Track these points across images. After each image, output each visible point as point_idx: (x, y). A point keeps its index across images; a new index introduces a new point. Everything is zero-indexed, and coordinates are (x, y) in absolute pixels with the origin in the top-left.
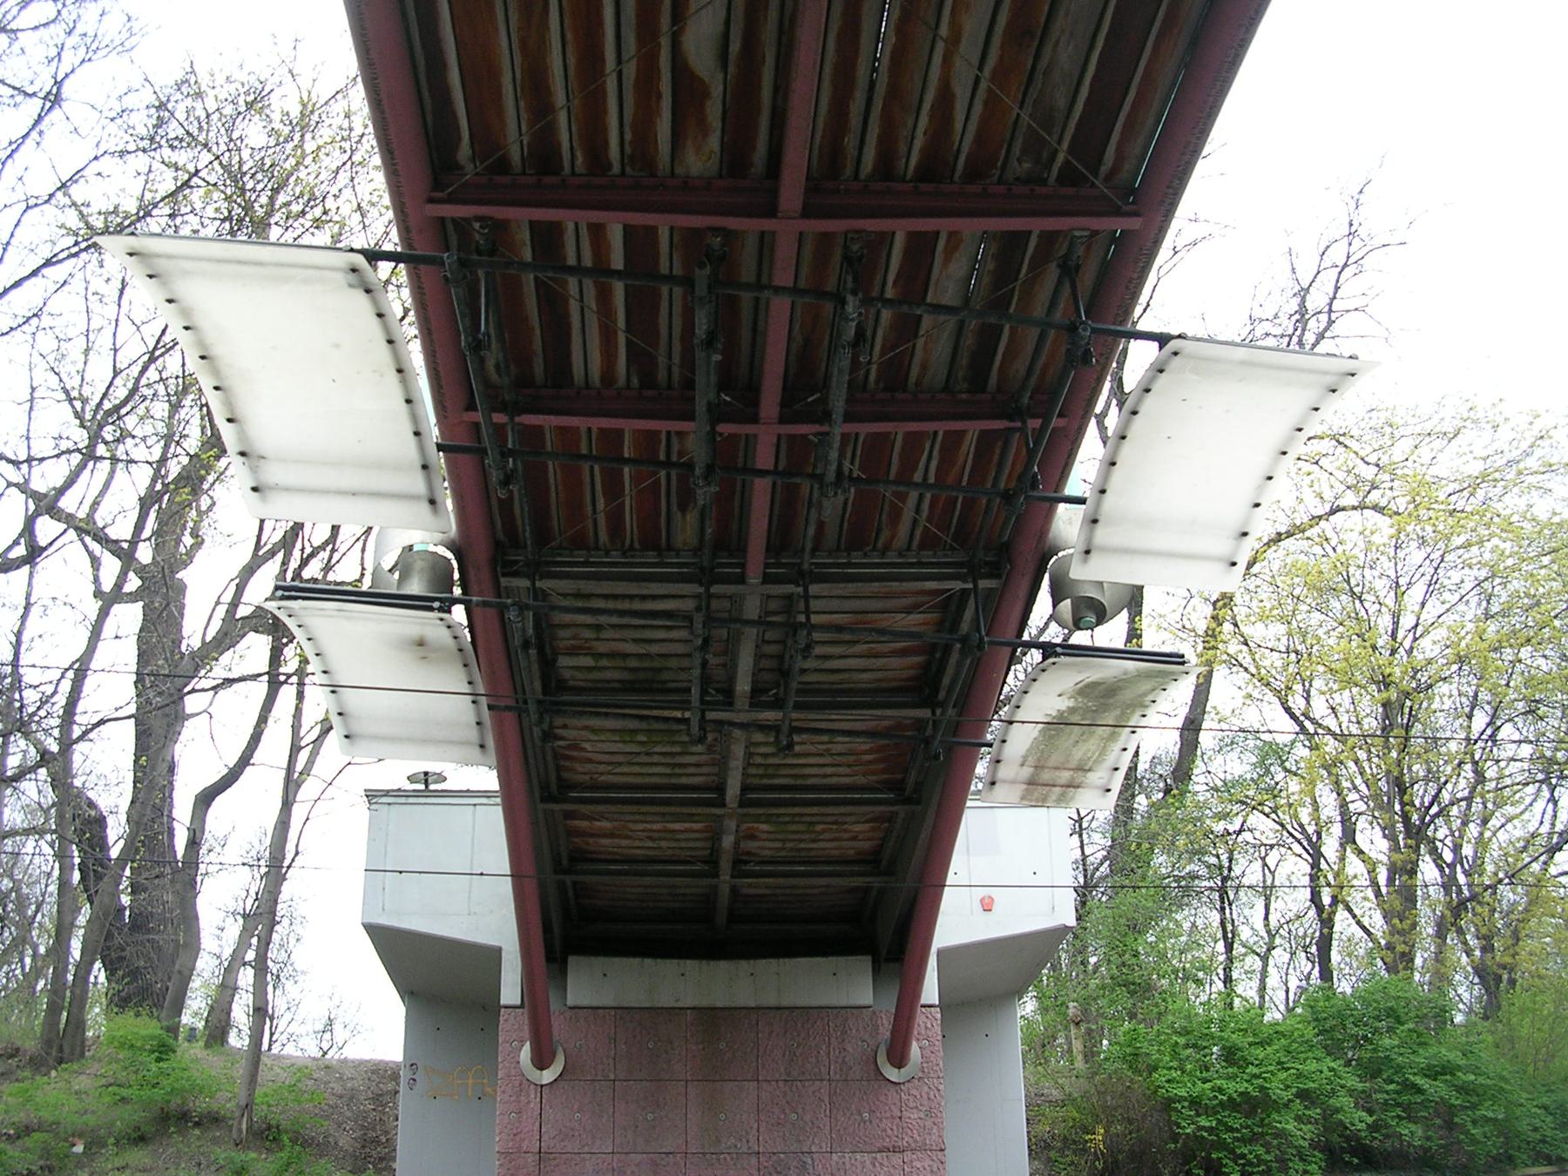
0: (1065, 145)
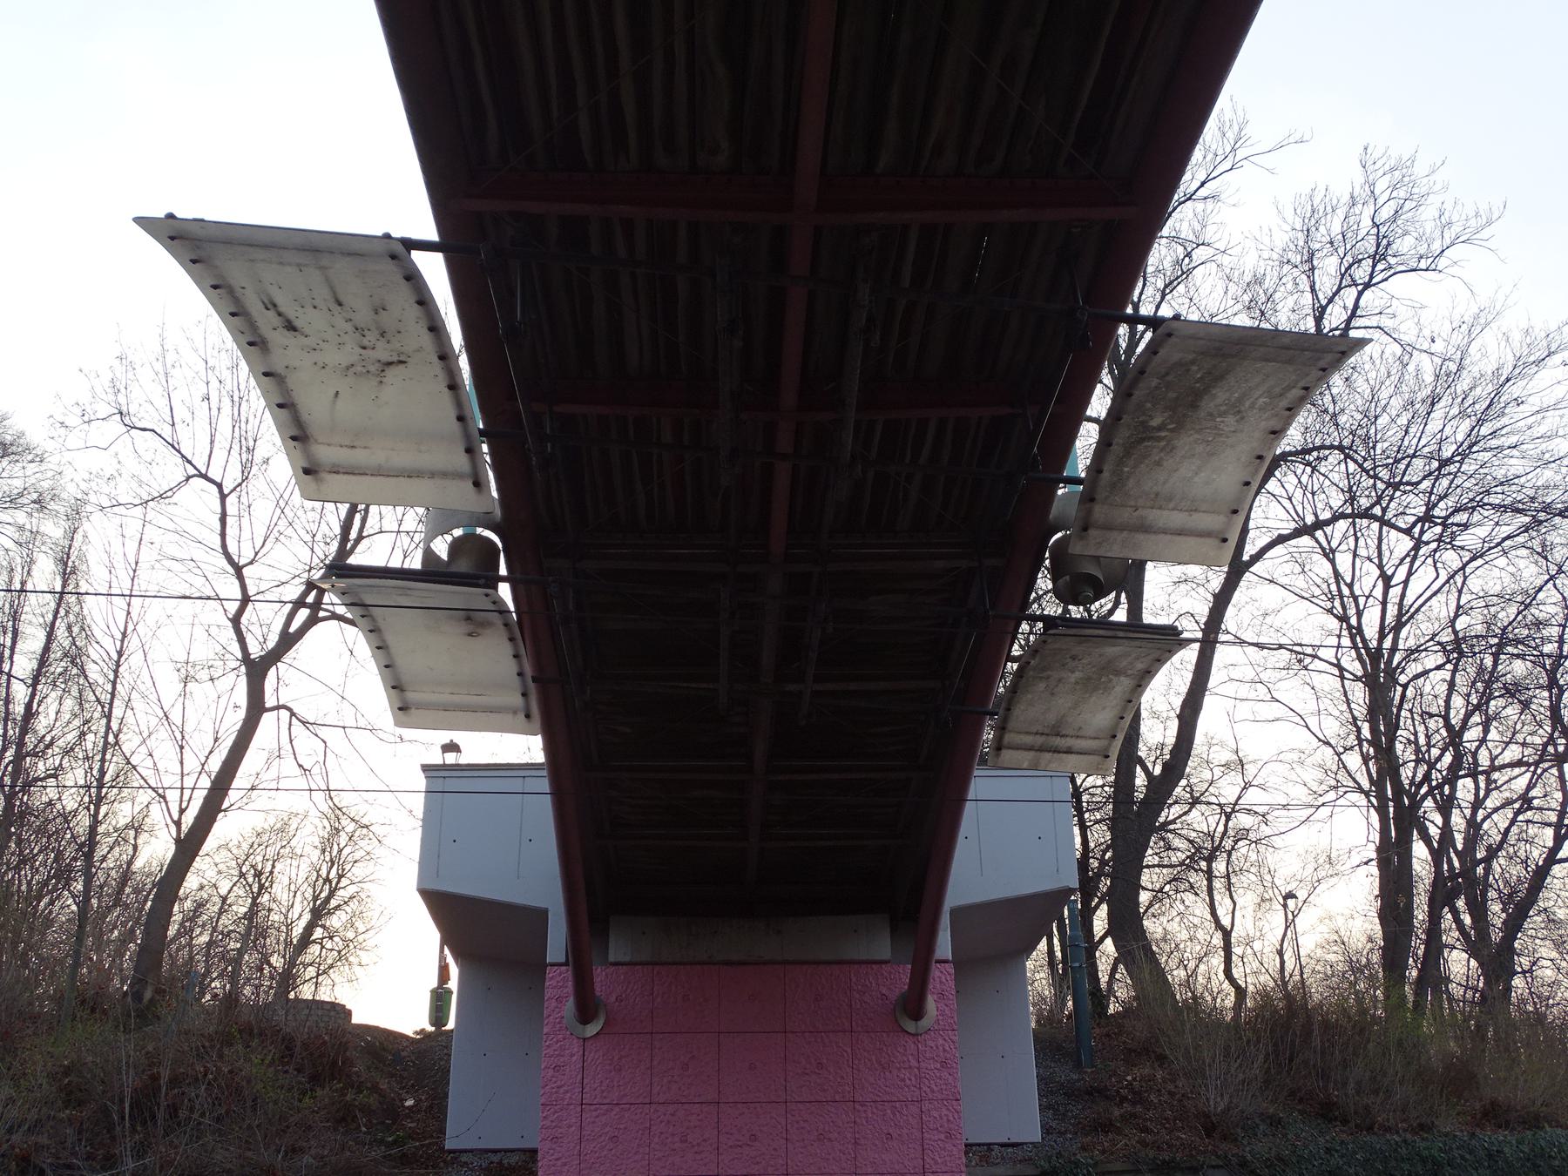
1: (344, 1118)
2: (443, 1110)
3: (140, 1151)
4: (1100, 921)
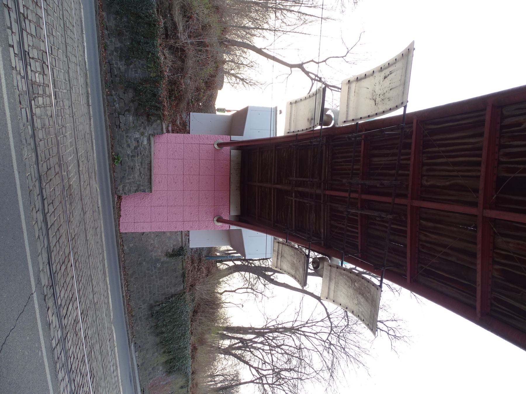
0: (428, 268)
1: (198, 89)
2: (199, 112)
3: (192, 44)
4: (239, 263)
